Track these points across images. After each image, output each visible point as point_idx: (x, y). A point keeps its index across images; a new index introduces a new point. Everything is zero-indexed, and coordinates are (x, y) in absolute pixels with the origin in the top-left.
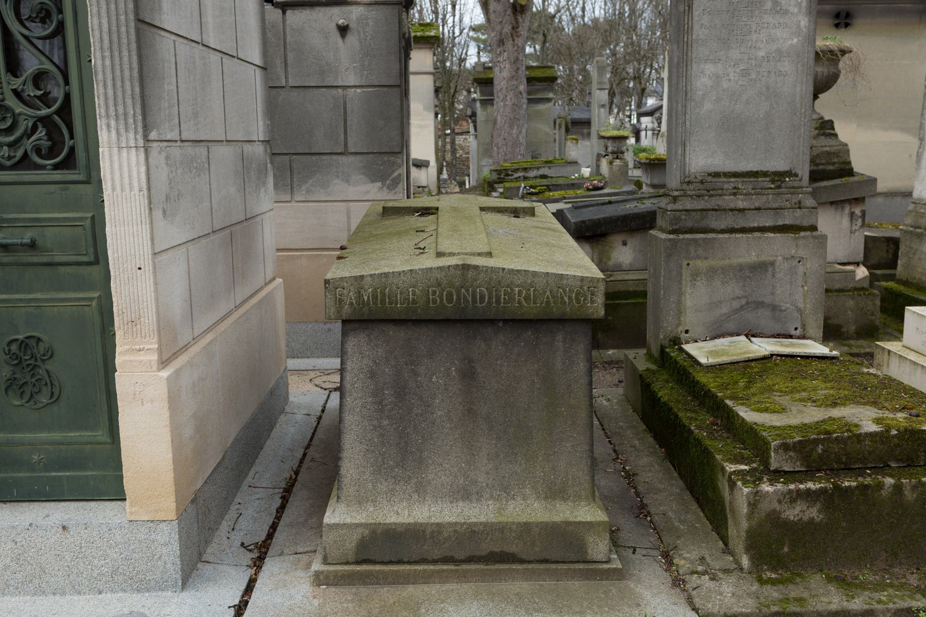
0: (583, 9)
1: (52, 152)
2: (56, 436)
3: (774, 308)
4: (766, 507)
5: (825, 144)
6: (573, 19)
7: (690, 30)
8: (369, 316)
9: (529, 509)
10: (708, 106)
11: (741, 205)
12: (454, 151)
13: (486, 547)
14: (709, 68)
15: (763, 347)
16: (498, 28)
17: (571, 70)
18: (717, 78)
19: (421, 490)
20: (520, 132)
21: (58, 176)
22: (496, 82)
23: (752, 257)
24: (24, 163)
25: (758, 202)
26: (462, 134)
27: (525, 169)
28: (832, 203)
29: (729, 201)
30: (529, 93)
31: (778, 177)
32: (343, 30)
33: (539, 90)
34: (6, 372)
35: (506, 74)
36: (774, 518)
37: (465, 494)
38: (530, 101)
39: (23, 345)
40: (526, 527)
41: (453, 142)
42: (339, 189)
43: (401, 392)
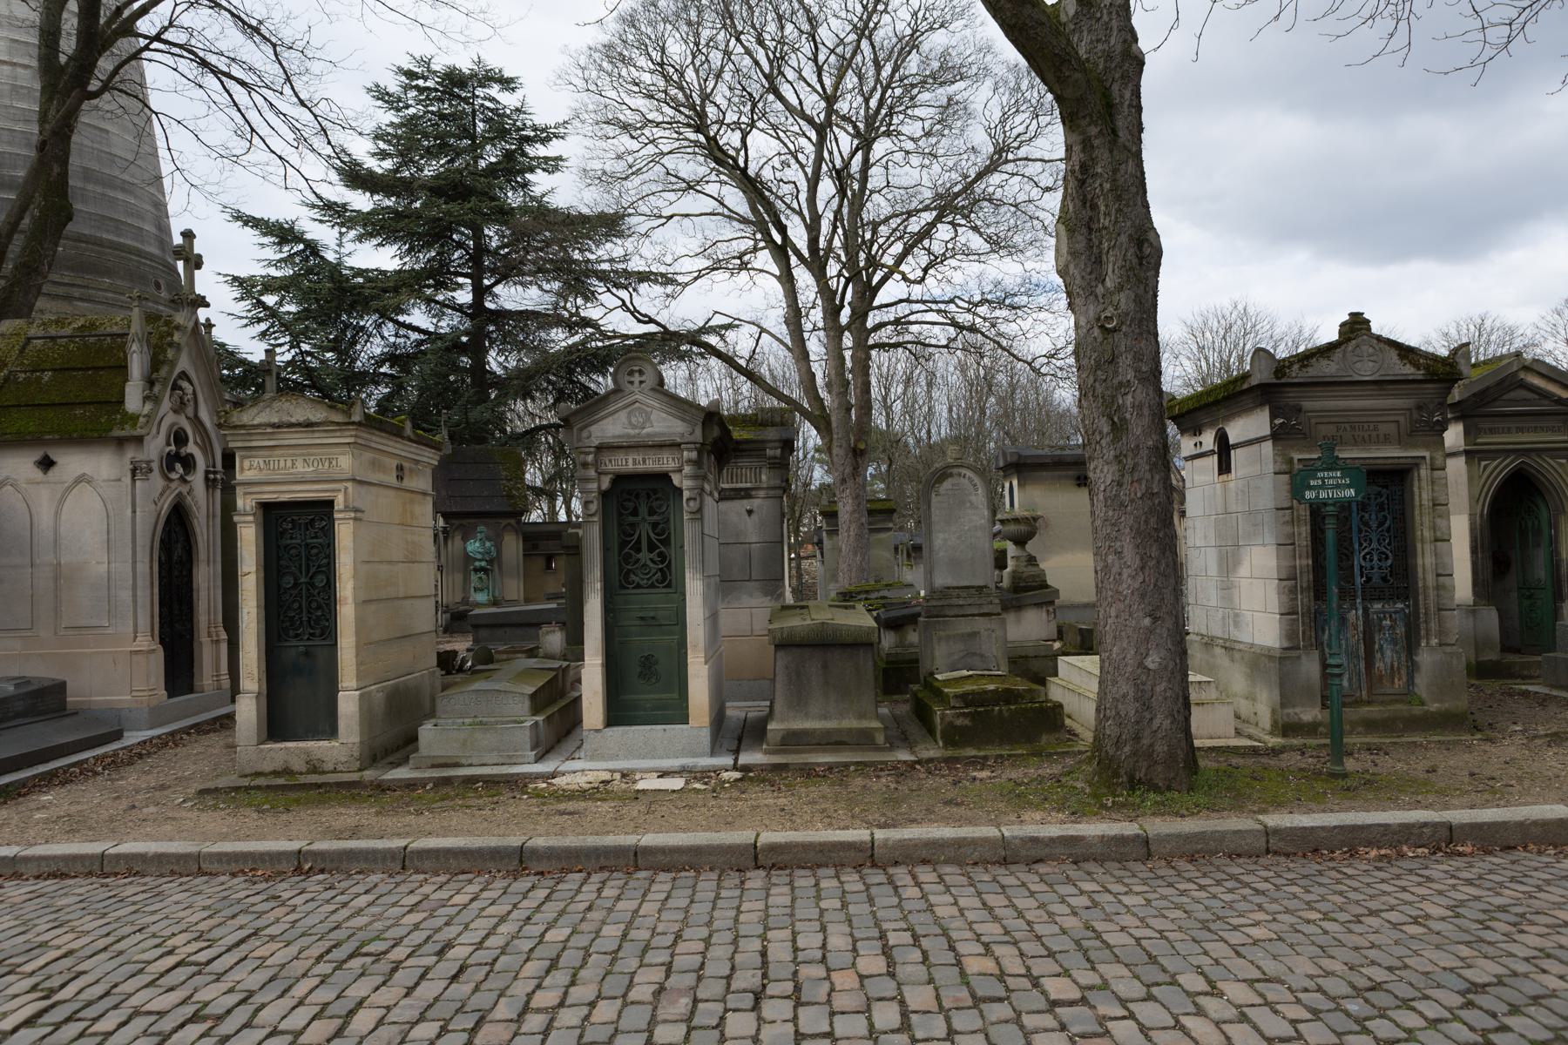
0: (929, 432)
3: (982, 656)
4: (947, 719)
5: (1031, 570)
6: (918, 441)
8: (785, 644)
9: (851, 723)
12: (800, 576)
13: (834, 739)
14: (941, 536)
15: (965, 673)
18: (945, 540)
19: (807, 716)
23: (969, 630)
24: (652, 586)
25: (969, 601)
26: (807, 558)
27: (867, 592)
29: (955, 601)
31: (980, 589)
35: (849, 508)
36: (951, 724)
37: (825, 717)
39: (647, 658)
40: (850, 730)
41: (799, 567)
42: (747, 601)
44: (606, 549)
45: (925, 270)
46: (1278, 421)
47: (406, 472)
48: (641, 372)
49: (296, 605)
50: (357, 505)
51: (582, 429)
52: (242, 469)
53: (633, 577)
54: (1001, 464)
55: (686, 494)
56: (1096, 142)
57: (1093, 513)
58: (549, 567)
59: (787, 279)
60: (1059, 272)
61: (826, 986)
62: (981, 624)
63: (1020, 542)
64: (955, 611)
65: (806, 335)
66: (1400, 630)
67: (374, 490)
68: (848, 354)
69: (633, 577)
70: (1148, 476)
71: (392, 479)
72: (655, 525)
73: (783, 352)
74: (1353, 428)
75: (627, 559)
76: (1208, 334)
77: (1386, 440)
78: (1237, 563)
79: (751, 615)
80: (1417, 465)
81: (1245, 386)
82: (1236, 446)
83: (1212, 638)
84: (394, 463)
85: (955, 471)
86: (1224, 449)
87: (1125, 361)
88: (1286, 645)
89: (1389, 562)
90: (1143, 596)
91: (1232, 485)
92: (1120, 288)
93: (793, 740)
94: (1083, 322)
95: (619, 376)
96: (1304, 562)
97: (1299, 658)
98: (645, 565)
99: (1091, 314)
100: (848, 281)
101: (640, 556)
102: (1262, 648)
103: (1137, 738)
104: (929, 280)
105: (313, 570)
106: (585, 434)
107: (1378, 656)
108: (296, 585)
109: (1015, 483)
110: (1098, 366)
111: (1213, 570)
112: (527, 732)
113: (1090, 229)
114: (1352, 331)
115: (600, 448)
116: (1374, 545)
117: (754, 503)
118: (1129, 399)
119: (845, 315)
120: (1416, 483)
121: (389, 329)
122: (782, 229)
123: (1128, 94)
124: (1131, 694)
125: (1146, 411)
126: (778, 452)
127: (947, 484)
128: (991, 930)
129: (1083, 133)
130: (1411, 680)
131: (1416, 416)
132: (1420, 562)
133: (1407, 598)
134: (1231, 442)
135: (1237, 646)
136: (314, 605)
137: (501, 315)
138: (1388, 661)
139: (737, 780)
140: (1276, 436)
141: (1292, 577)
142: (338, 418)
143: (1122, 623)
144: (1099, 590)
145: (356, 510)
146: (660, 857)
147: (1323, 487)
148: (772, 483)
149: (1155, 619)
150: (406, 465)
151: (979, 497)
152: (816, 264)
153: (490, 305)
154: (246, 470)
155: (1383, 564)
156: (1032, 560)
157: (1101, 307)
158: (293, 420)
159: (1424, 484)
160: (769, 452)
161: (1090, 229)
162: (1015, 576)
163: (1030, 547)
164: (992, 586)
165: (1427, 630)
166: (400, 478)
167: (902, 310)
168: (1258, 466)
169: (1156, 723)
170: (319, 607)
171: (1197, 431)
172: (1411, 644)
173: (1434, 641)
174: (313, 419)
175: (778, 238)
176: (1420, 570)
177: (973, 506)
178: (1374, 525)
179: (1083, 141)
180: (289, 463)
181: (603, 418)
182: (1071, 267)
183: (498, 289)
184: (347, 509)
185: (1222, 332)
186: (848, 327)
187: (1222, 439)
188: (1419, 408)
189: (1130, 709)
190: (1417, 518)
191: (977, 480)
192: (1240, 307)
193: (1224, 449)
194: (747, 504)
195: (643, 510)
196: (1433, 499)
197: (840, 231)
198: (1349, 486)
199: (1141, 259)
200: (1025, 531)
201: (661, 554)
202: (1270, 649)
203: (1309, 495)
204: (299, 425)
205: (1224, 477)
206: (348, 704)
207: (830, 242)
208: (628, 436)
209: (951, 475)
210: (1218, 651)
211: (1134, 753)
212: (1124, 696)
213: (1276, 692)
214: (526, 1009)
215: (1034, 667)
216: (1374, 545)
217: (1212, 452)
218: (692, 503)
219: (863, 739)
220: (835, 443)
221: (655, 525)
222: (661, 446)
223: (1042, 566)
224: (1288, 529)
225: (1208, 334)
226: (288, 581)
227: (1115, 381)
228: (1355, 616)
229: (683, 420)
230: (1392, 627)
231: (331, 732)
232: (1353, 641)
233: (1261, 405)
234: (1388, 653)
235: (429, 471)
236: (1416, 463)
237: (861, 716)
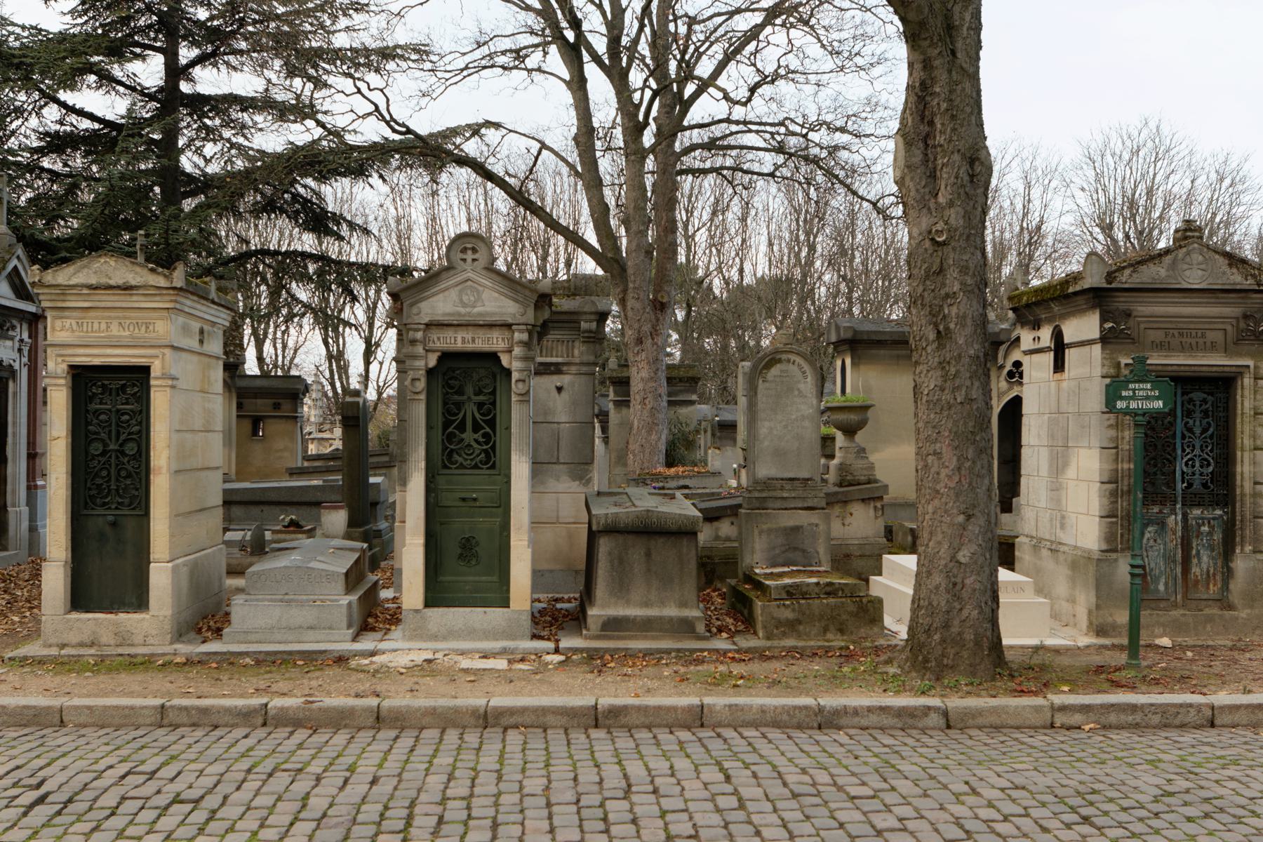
0: (741, 271)
1: (486, 463)
2: (477, 578)
3: (804, 551)
7: (756, 404)
9: (671, 611)
10: (766, 443)
11: (785, 495)
14: (767, 424)
16: (636, 326)
17: (725, 347)
19: (628, 603)
20: (659, 438)
21: (488, 472)
22: (633, 383)
23: (791, 523)
24: (476, 467)
28: (863, 500)
29: (778, 494)
30: (669, 395)
32: (559, 389)
33: (681, 391)
34: (459, 551)
35: (644, 374)
37: (647, 604)
38: (670, 403)
43: (621, 561)
44: (429, 428)
45: (753, 90)
46: (1108, 325)
47: (206, 335)
48: (474, 250)
49: (104, 473)
50: (173, 372)
51: (412, 305)
52: (53, 329)
53: (456, 457)
54: (833, 339)
55: (515, 376)
56: (937, 63)
57: (916, 415)
58: (255, 433)
59: (578, 84)
60: (896, 183)
61: (679, 788)
62: (803, 518)
63: (850, 431)
64: (778, 504)
65: (598, 154)
66: (1218, 536)
67: (184, 355)
68: (649, 181)
69: (456, 457)
70: (968, 383)
71: (193, 343)
72: (480, 405)
73: (567, 179)
74: (1181, 335)
75: (450, 438)
76: (1109, 159)
77: (1213, 347)
78: (1066, 464)
79: (567, 498)
80: (1241, 374)
81: (1078, 288)
82: (1071, 345)
83: (1040, 540)
84: (196, 326)
85: (784, 356)
86: (1060, 348)
87: (952, 273)
88: (1104, 547)
89: (1211, 469)
90: (957, 495)
91: (1065, 385)
92: (951, 204)
93: (613, 626)
94: (916, 232)
95: (452, 253)
96: (1126, 466)
97: (1116, 560)
98: (469, 446)
99: (924, 226)
100: (655, 94)
101: (463, 436)
102: (1084, 550)
103: (946, 626)
104: (757, 101)
105: (123, 437)
106: (415, 310)
107: (1195, 561)
108: (104, 453)
109: (848, 361)
110: (927, 277)
111: (1044, 471)
112: (344, 611)
113: (927, 145)
114: (1186, 238)
115: (429, 325)
116: (1197, 451)
117: (564, 380)
118: (954, 310)
119: (648, 139)
120: (1239, 392)
121: (52, 113)
122: (576, 24)
123: (968, 17)
124: (943, 585)
125: (969, 322)
126: (594, 324)
127: (775, 371)
128: (805, 762)
129: (923, 53)
130: (1226, 586)
131: (1242, 325)
132: (1239, 469)
133: (1226, 505)
134: (1066, 341)
135: (1062, 548)
136: (123, 473)
137: (199, 103)
138: (1204, 566)
139: (561, 663)
140: (1105, 339)
141: (1113, 480)
142: (162, 282)
143: (938, 518)
144: (919, 489)
145: (174, 379)
146: (840, 497)
147: (1133, 398)
148: (586, 358)
149: (969, 517)
150: (206, 328)
151: (808, 384)
152: (618, 77)
153: (185, 87)
154: (59, 330)
155: (1205, 471)
156: (862, 451)
157: (933, 220)
158: (112, 282)
159: (1246, 392)
160: (584, 325)
161: (927, 145)
162: (842, 468)
163: (860, 437)
164: (818, 479)
165: (1242, 537)
166: (201, 342)
167: (718, 131)
168: (1087, 366)
169: (965, 613)
170: (129, 476)
171: (1036, 325)
172: (1227, 550)
173: (1248, 548)
174: (133, 283)
175: (570, 35)
176: (1238, 478)
177: (801, 394)
178: (1198, 431)
179: (924, 61)
180: (103, 326)
181: (434, 295)
182: (907, 179)
183: (197, 71)
184: (165, 376)
185: (1126, 156)
186: (653, 149)
187: (1058, 336)
188: (1246, 317)
189: (941, 600)
190: (1239, 426)
191: (806, 367)
192: (1152, 125)
193: (1060, 348)
194: (557, 380)
195: (469, 390)
196: (1255, 408)
197: (647, 30)
198: (1158, 398)
199: (972, 176)
200: (853, 419)
201: (486, 435)
202: (1090, 551)
203: (1120, 405)
204: (118, 287)
205: (1058, 376)
206: (161, 577)
207: (636, 41)
208: (459, 314)
209: (780, 361)
210: (1045, 553)
211: (943, 641)
212: (937, 588)
213: (1093, 594)
214: (444, 800)
215: (859, 563)
216: (1197, 451)
217: (1047, 349)
218: (520, 385)
219: (685, 627)
220: (630, 294)
221: (480, 405)
222: (491, 326)
223: (874, 458)
224: (1112, 433)
225: (1109, 159)
226: (96, 448)
227: (943, 292)
228: (1175, 521)
229: (516, 301)
230: (1210, 534)
231: (140, 601)
232: (1171, 546)
233: (1093, 307)
234: (1205, 559)
235: (221, 333)
236: (1239, 372)
237: (683, 604)
